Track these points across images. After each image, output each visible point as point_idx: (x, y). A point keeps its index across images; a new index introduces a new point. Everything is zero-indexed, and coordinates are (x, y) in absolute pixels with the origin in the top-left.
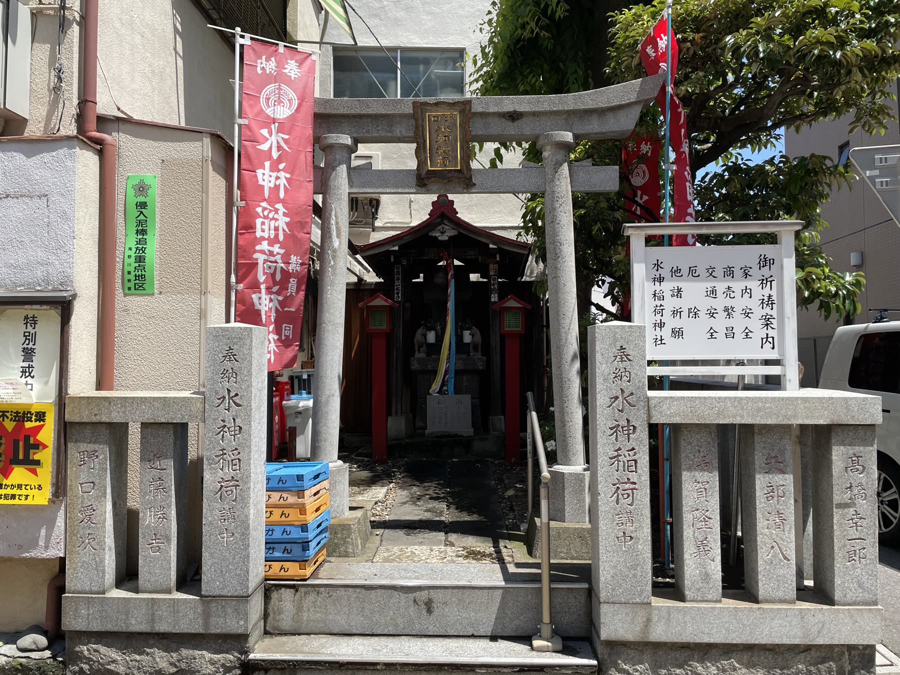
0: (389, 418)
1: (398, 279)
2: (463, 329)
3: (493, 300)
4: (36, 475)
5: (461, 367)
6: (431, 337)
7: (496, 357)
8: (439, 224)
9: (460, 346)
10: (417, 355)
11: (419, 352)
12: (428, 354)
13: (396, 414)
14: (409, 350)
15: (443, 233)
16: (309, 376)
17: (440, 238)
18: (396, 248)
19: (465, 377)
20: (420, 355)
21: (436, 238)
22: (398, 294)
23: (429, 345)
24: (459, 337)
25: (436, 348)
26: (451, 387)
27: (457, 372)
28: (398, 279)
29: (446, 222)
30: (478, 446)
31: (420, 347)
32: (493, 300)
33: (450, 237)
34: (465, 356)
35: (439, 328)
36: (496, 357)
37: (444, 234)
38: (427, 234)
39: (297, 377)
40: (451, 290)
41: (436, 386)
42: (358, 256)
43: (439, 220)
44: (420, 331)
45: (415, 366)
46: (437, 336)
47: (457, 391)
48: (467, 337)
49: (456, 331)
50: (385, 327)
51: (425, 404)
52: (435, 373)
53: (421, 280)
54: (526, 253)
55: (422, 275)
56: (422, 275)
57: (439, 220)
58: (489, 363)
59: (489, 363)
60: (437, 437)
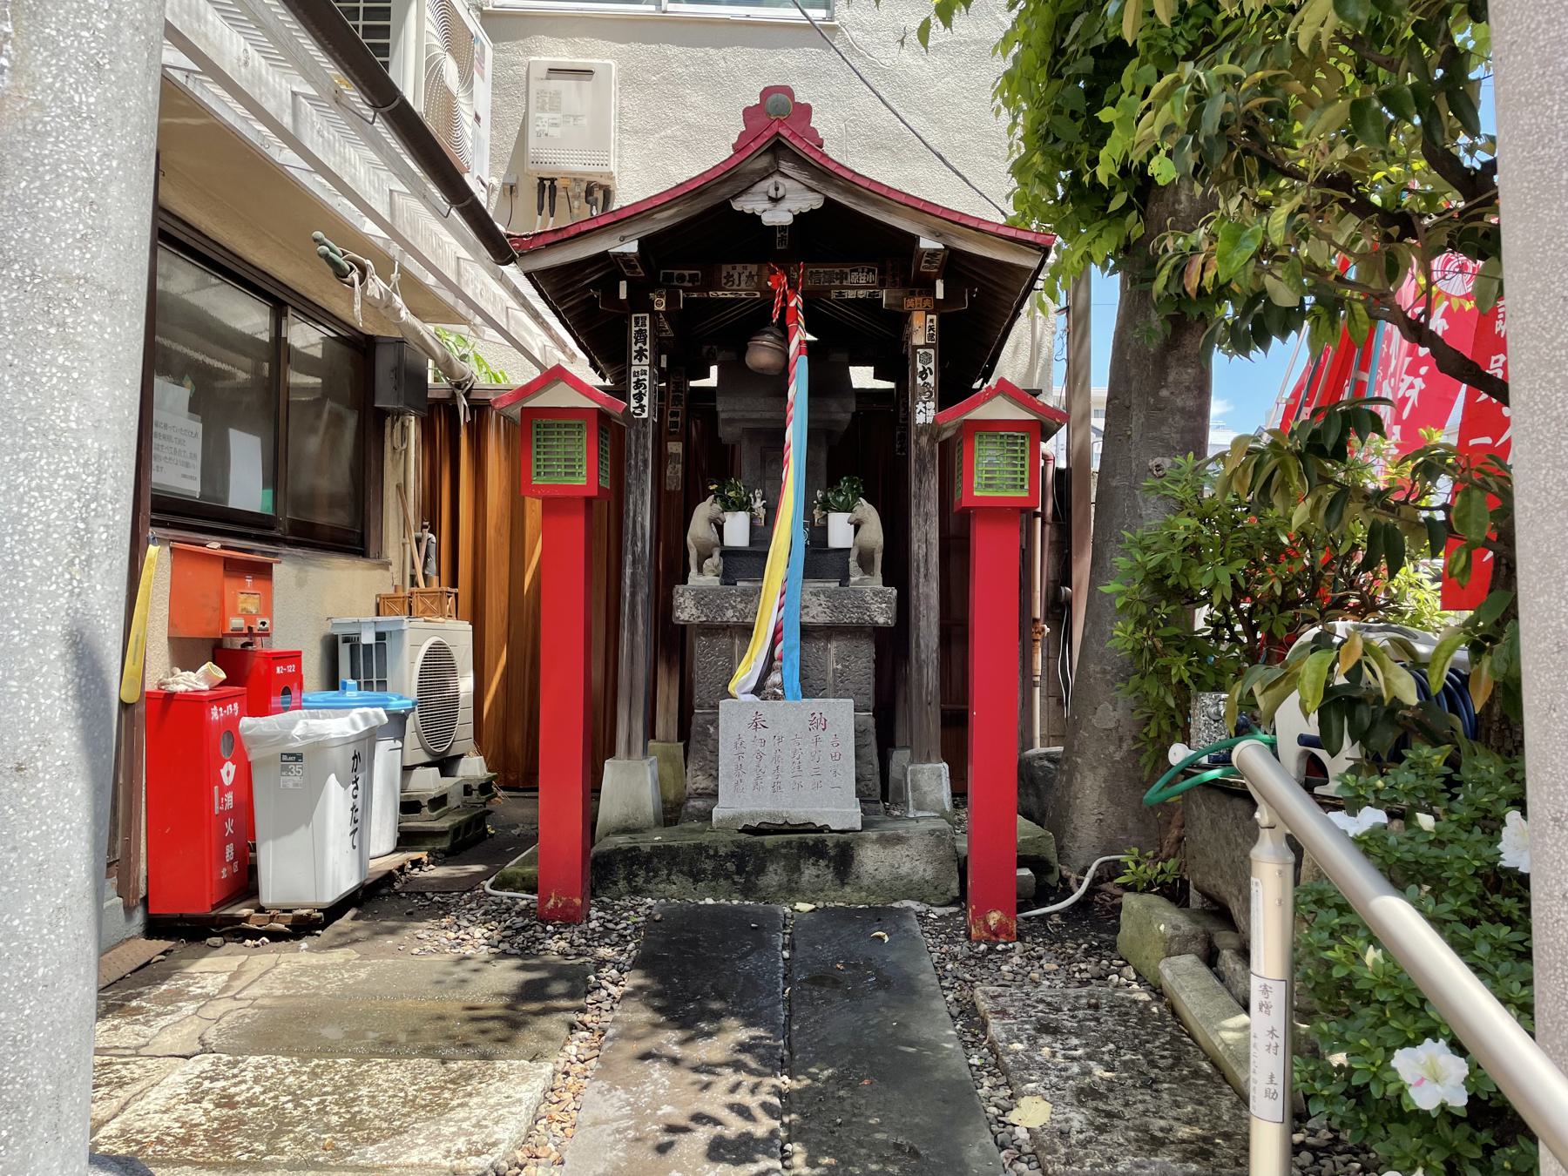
0: (609, 765)
1: (641, 353)
2: (826, 506)
3: (920, 419)
4: (1490, 591)
5: (819, 614)
6: (737, 530)
7: (927, 591)
8: (765, 175)
9: (819, 558)
10: (694, 578)
11: (700, 570)
12: (728, 577)
13: (629, 752)
14: (672, 565)
15: (775, 200)
16: (380, 636)
17: (768, 219)
18: (632, 247)
19: (833, 647)
20: (703, 579)
21: (755, 219)
22: (639, 397)
23: (729, 554)
24: (817, 537)
25: (745, 564)
26: (788, 674)
27: (807, 632)
28: (641, 353)
29: (785, 166)
30: (872, 860)
31: (704, 556)
32: (920, 419)
33: (800, 218)
34: (834, 585)
35: (758, 504)
36: (927, 591)
37: (781, 203)
38: (726, 204)
39: (346, 640)
40: (798, 389)
41: (747, 672)
42: (512, 271)
43: (763, 162)
44: (705, 510)
45: (686, 610)
46: (753, 528)
47: (809, 689)
48: (840, 531)
49: (808, 513)
50: (582, 481)
51: (715, 722)
52: (746, 631)
53: (712, 380)
54: (1033, 263)
55: (714, 370)
56: (714, 370)
57: (763, 162)
58: (904, 606)
59: (904, 606)
60: (747, 830)
